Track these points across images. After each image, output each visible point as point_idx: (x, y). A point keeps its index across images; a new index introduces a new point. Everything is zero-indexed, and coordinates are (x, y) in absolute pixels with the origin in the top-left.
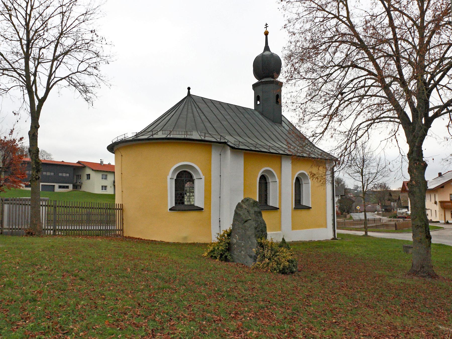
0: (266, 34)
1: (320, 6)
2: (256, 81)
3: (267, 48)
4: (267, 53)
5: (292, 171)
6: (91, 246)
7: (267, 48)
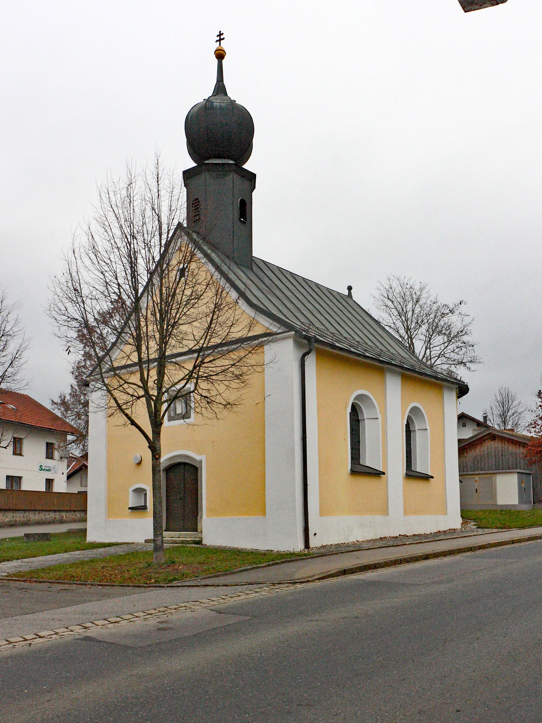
0: (220, 55)
1: (128, 319)
2: (192, 164)
3: (220, 88)
4: (218, 102)
5: (402, 404)
6: (403, 363)
7: (220, 88)
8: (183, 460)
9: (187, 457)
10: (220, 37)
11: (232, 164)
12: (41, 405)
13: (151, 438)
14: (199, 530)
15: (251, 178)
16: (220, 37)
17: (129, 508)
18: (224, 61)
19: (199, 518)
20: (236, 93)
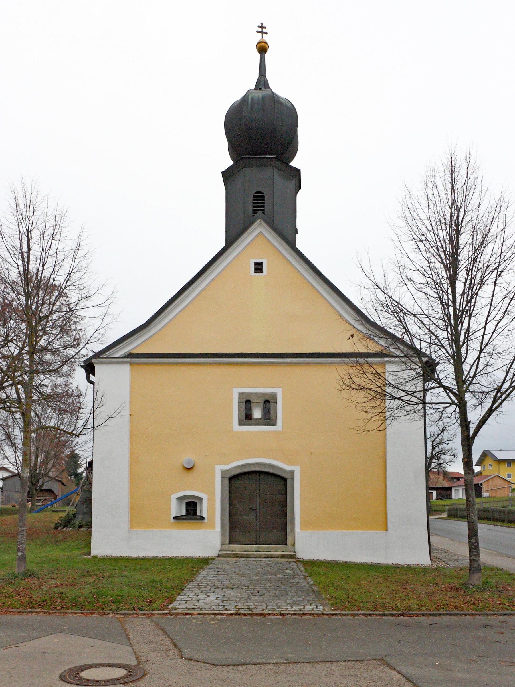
0: (262, 49)
3: (262, 82)
7: (262, 82)
8: (262, 469)
9: (271, 466)
10: (262, 29)
11: (469, 432)
12: (185, 354)
13: (453, 324)
14: (289, 543)
15: (296, 174)
16: (262, 29)
17: (175, 518)
18: (266, 55)
19: (288, 530)
20: (280, 86)
